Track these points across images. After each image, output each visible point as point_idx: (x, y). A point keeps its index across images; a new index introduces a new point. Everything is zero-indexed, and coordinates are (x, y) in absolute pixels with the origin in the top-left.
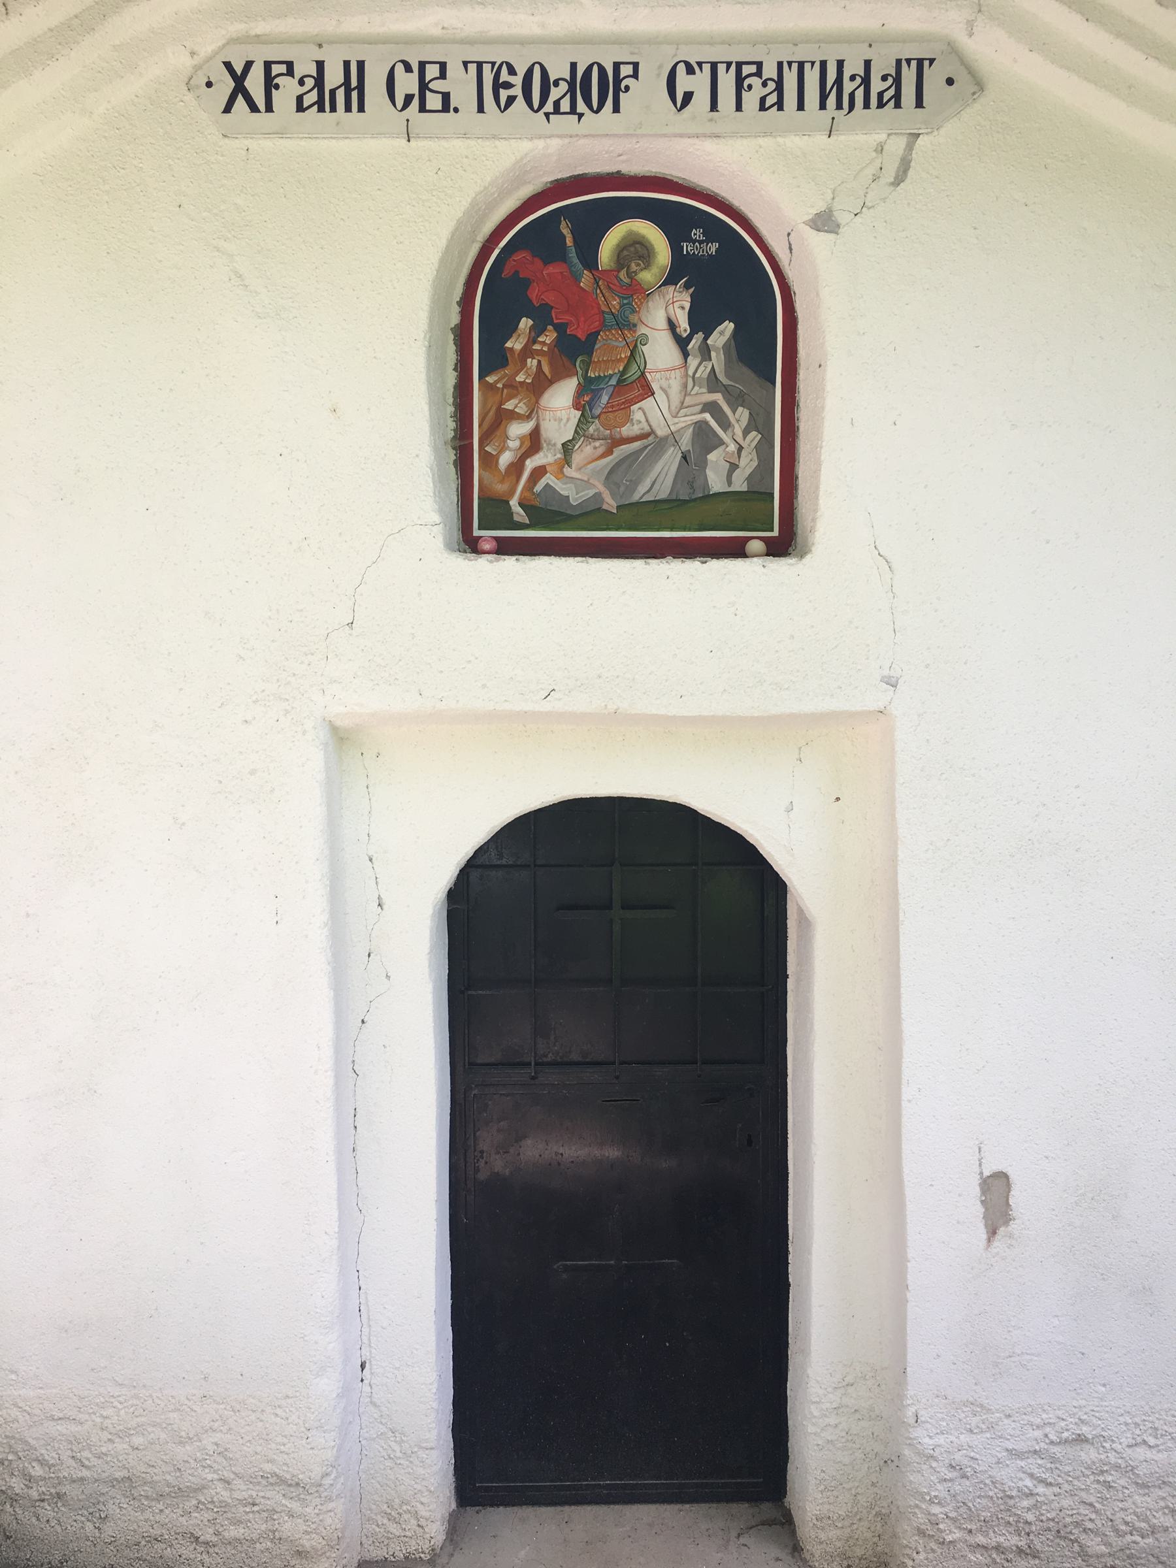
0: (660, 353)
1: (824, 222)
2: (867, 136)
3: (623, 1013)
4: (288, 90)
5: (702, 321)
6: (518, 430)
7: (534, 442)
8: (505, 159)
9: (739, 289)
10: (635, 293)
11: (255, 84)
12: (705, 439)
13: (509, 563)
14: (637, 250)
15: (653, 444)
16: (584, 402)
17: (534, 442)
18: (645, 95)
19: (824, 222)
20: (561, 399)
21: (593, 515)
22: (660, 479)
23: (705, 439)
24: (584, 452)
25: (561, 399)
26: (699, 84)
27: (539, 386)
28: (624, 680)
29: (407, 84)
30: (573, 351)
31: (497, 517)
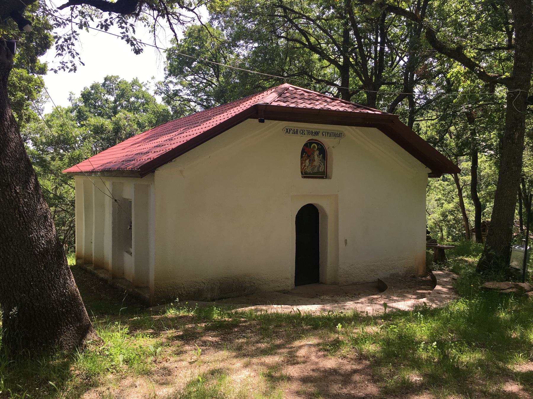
0: (316, 157)
1: (333, 147)
2: (337, 139)
3: (309, 220)
4: (291, 132)
5: (320, 154)
6: (304, 164)
7: (305, 166)
8: (306, 139)
9: (323, 151)
10: (314, 151)
11: (288, 131)
12: (320, 166)
13: (307, 180)
14: (314, 147)
15: (315, 166)
16: (309, 161)
17: (305, 166)
18: (320, 134)
19: (333, 147)
20: (307, 161)
21: (310, 174)
22: (316, 170)
23: (320, 166)
24: (309, 167)
25: (307, 161)
26: (324, 134)
27: (306, 160)
28: (313, 191)
29: (301, 132)
30: (309, 156)
31: (306, 175)
